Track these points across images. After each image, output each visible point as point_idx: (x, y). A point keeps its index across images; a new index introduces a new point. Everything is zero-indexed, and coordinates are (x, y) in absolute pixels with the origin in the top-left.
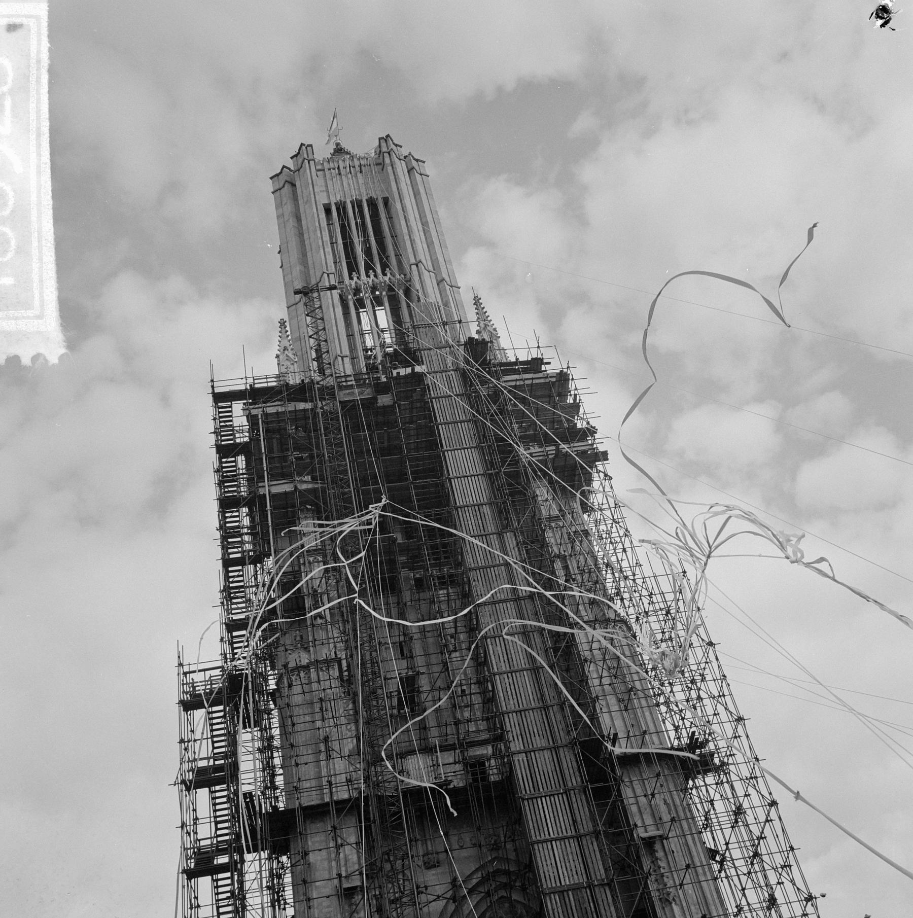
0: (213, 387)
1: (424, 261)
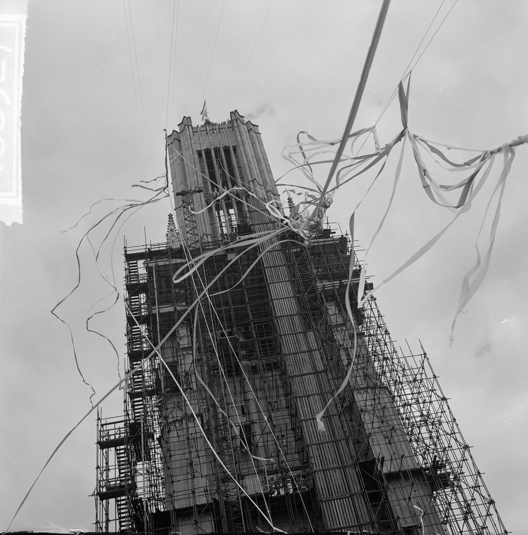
0: (125, 251)
1: (257, 180)
